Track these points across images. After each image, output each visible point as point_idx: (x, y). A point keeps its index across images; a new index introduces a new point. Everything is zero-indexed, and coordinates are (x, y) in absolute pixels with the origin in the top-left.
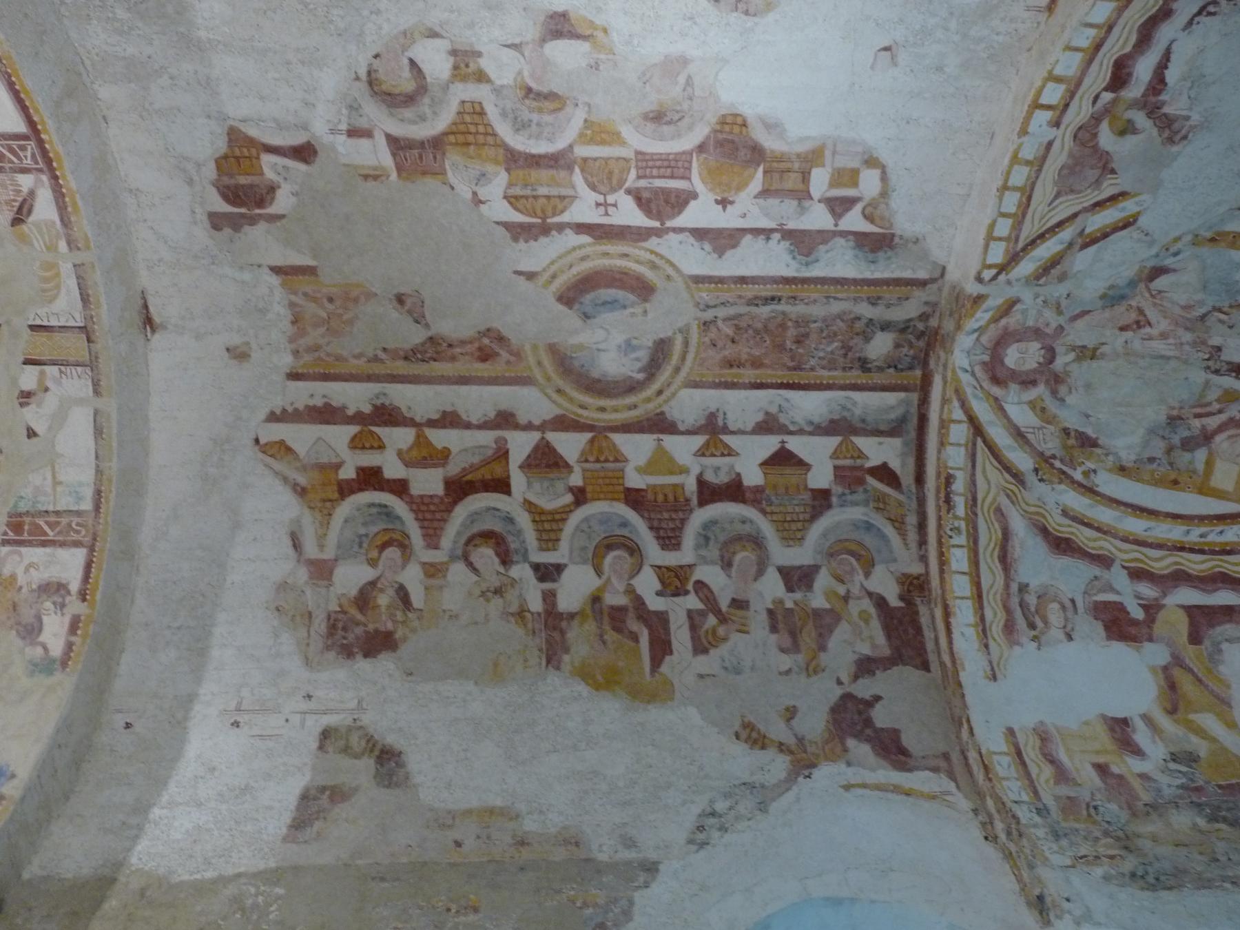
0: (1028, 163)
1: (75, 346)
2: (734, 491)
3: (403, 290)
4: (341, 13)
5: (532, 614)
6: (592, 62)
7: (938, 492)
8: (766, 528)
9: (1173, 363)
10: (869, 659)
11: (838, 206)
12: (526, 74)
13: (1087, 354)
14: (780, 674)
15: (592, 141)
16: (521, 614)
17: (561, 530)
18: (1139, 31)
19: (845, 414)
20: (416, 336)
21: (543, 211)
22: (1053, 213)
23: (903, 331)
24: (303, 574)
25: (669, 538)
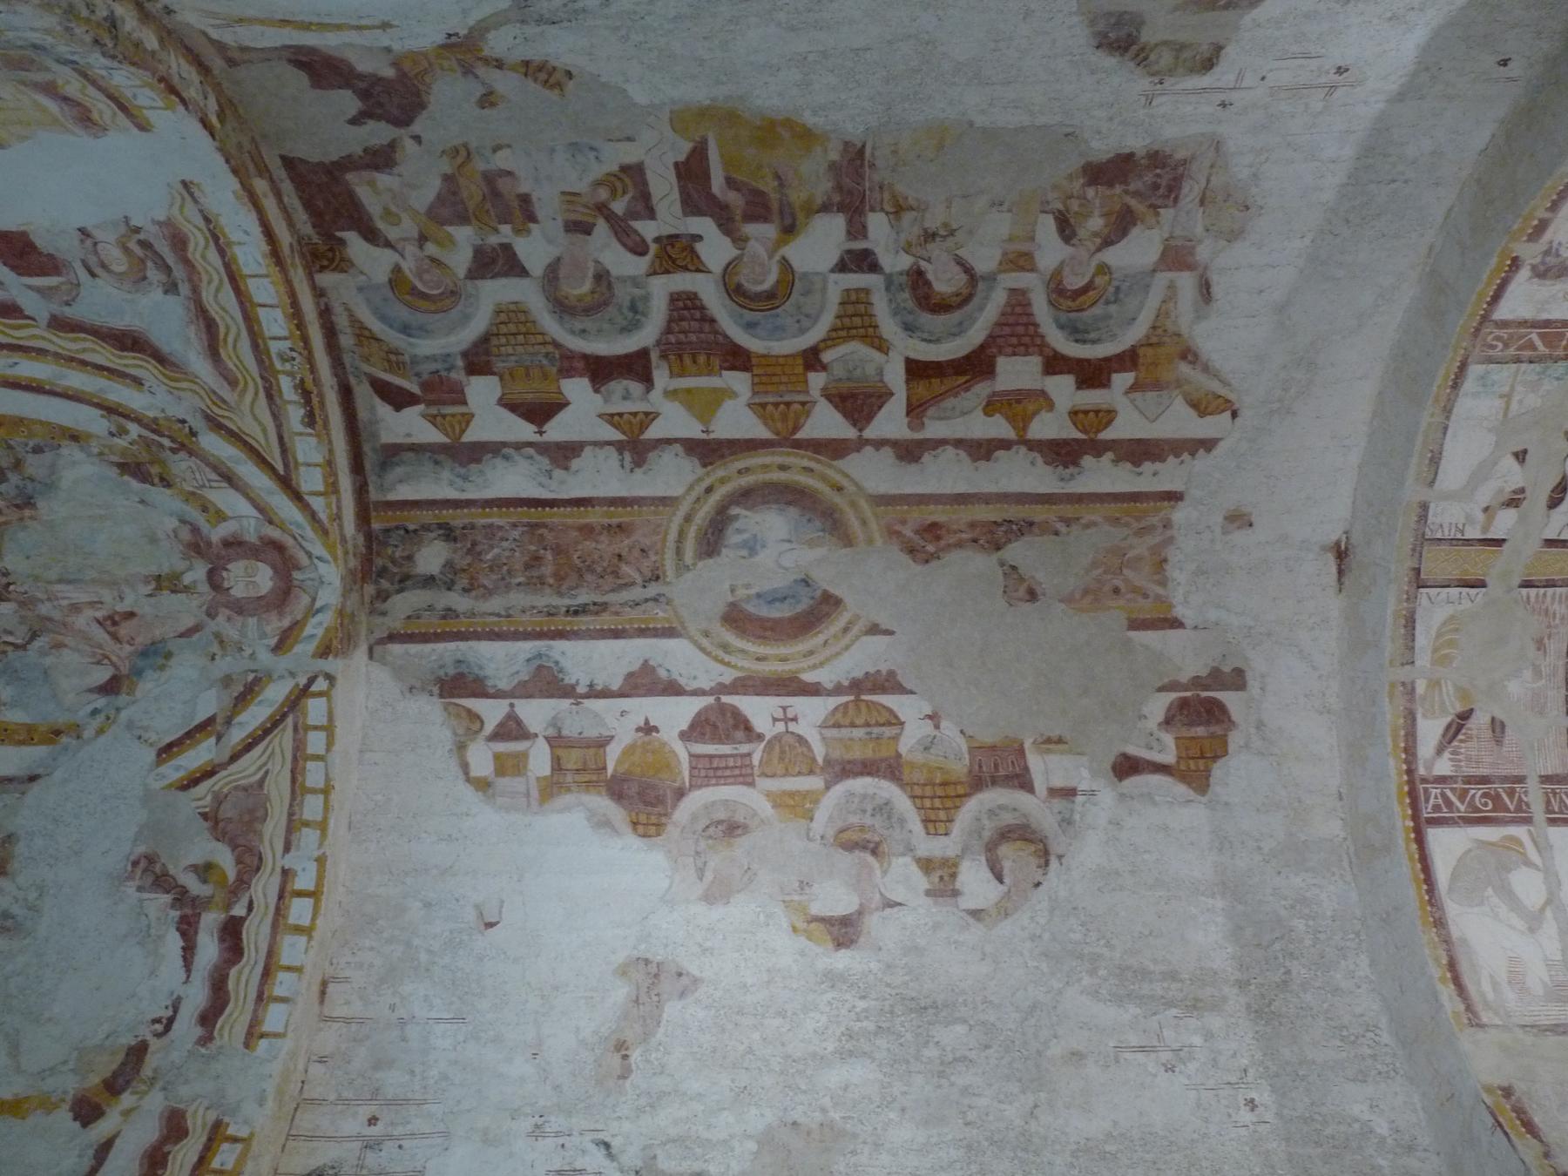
0: (307, 824)
1: (1437, 564)
2: (601, 371)
3: (1028, 607)
4: (1072, 935)
5: (882, 210)
6: (807, 890)
7: (322, 404)
8: (551, 325)
9: (53, 574)
10: (377, 168)
11: (512, 729)
12: (878, 872)
13: (166, 583)
14: (509, 146)
15: (805, 795)
16: (899, 209)
17: (838, 317)
18: (227, 993)
19: (463, 471)
20: (1016, 552)
21: (858, 709)
22: (259, 763)
23: (405, 578)
24: (1203, 253)
25: (686, 308)
